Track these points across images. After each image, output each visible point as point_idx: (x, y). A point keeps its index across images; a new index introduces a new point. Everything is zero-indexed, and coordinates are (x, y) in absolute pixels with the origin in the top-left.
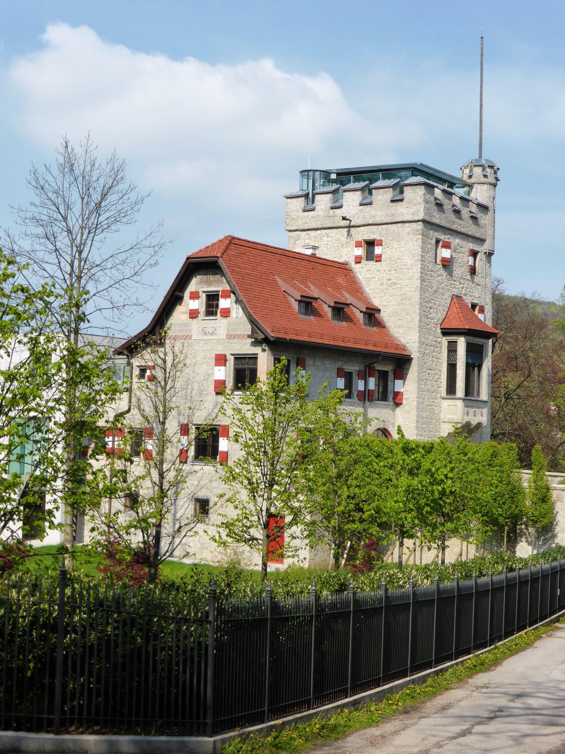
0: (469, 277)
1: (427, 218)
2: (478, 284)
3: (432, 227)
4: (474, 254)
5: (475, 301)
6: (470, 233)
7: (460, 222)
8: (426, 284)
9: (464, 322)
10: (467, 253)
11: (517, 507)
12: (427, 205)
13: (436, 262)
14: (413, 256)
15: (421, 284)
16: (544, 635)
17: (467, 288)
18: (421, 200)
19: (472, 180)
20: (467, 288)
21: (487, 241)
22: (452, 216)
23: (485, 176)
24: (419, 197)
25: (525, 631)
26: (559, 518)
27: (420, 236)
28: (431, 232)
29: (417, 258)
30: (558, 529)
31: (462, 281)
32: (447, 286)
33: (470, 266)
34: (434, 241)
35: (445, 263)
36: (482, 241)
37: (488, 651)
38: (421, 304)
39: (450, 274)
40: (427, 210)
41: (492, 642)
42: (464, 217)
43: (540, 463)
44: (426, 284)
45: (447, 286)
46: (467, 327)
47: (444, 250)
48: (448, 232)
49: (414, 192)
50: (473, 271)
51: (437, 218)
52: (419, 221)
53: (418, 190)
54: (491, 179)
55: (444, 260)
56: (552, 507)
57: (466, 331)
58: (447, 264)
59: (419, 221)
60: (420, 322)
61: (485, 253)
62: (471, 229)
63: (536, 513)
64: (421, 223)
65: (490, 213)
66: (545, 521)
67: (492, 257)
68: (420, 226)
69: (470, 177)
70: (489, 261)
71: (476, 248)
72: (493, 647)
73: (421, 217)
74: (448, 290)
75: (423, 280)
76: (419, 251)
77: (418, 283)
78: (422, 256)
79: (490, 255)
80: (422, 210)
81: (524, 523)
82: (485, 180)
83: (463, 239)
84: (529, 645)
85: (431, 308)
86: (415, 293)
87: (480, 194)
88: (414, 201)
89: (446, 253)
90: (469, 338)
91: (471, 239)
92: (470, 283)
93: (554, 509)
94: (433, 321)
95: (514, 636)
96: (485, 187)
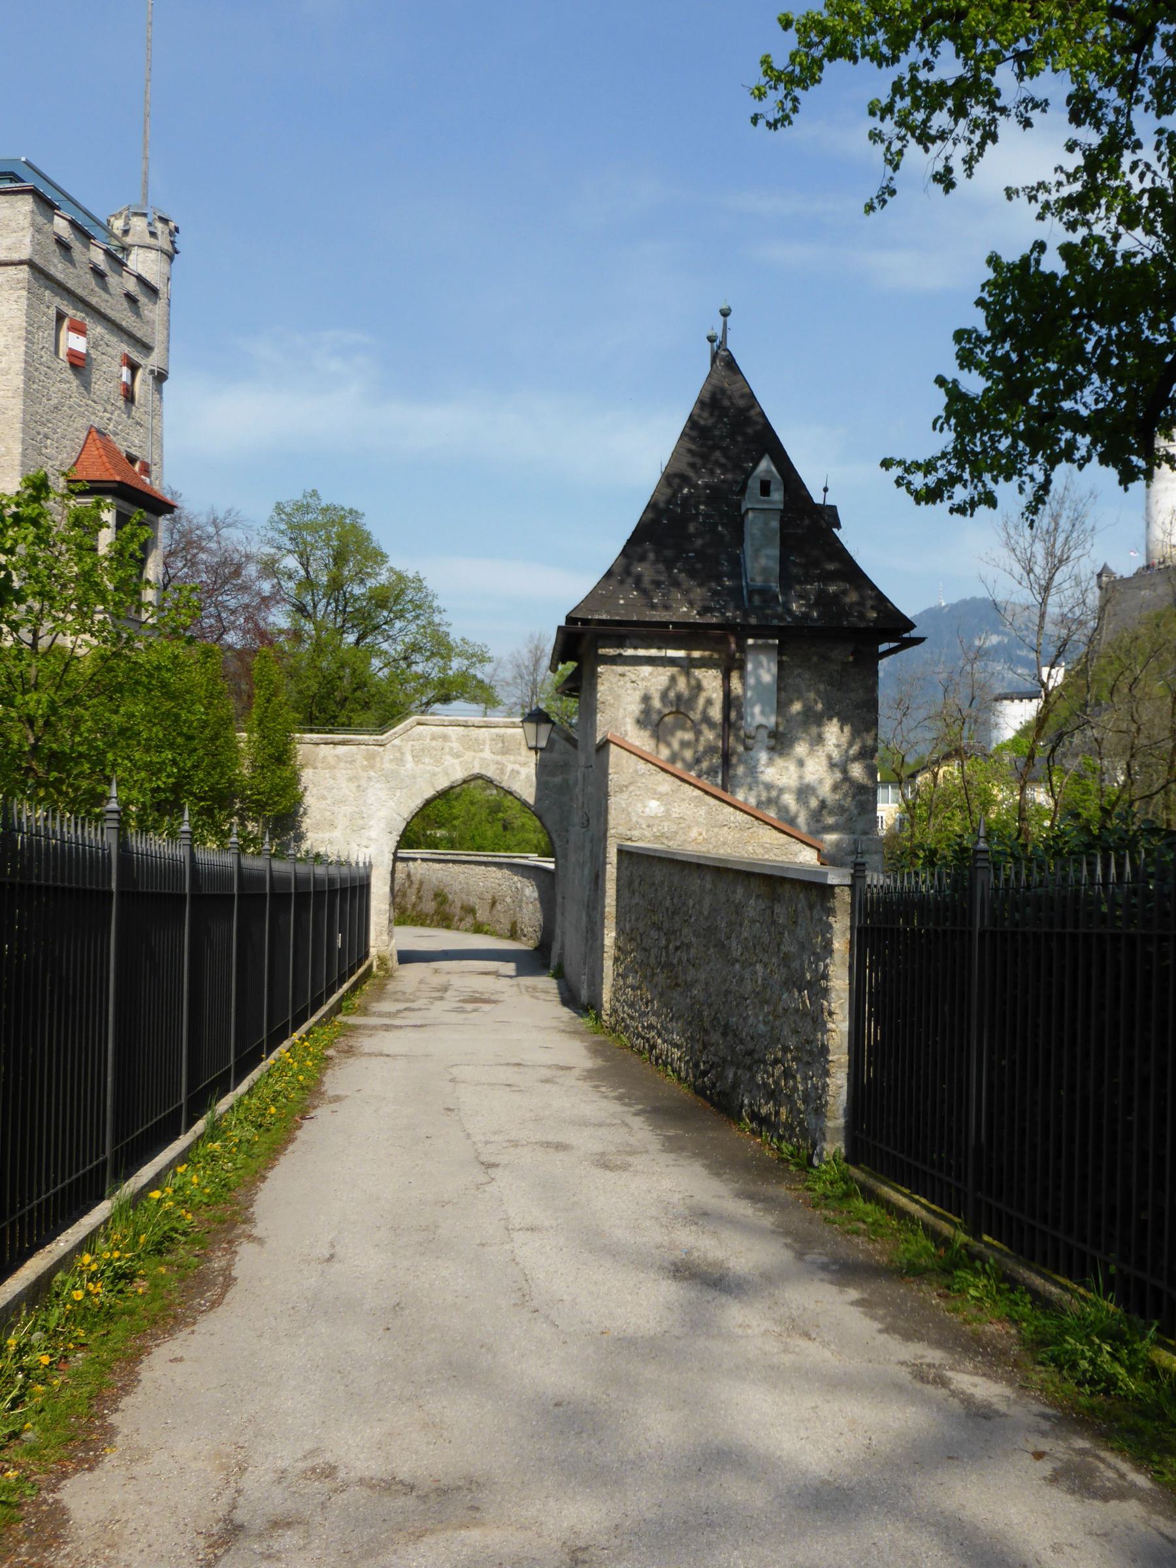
0: (121, 403)
1: (37, 260)
2: (138, 423)
3: (49, 283)
4: (134, 368)
5: (134, 451)
6: (124, 323)
7: (106, 296)
8: (35, 386)
9: (112, 471)
10: (118, 360)
11: (222, 774)
12: (36, 235)
13: (57, 352)
14: (10, 330)
15: (25, 383)
16: (331, 1052)
17: (118, 423)
18: (26, 223)
19: (128, 240)
20: (118, 423)
21: (156, 350)
22: (89, 278)
23: (153, 234)
24: (21, 217)
25: (286, 1044)
26: (309, 800)
27: (25, 293)
28: (47, 293)
29: (18, 333)
30: (307, 823)
31: (109, 408)
32: (80, 406)
33: (125, 383)
34: (52, 312)
35: (77, 362)
36: (147, 348)
37: (183, 1157)
38: (24, 422)
39: (86, 385)
40: (37, 245)
41: (199, 1105)
42: (112, 290)
43: (271, 682)
44: (35, 386)
45: (80, 406)
46: (118, 478)
47: (72, 335)
48: (81, 306)
49: (12, 206)
50: (129, 396)
51: (58, 268)
52: (21, 263)
53: (19, 203)
54: (163, 242)
55: (72, 354)
56: (295, 779)
57: (115, 485)
58: (79, 364)
59: (21, 263)
60: (24, 455)
61: (152, 372)
62: (125, 318)
63: (263, 787)
64: (25, 267)
65: (162, 303)
66: (285, 803)
67: (165, 385)
68: (24, 272)
69: (126, 232)
70: (159, 391)
71: (135, 356)
72: (200, 1126)
73: (25, 254)
74: (82, 415)
75: (29, 379)
76: (20, 320)
77: (19, 381)
78: (28, 332)
79: (160, 377)
80: (27, 240)
81: (237, 814)
82: (150, 241)
83: (111, 332)
84: (307, 1097)
85: (46, 437)
86: (14, 401)
87: (144, 262)
88: (13, 224)
89: (78, 343)
90: (121, 502)
91: (125, 337)
92: (125, 416)
93: (298, 781)
94: (50, 463)
95: (263, 1067)
96: (153, 255)
